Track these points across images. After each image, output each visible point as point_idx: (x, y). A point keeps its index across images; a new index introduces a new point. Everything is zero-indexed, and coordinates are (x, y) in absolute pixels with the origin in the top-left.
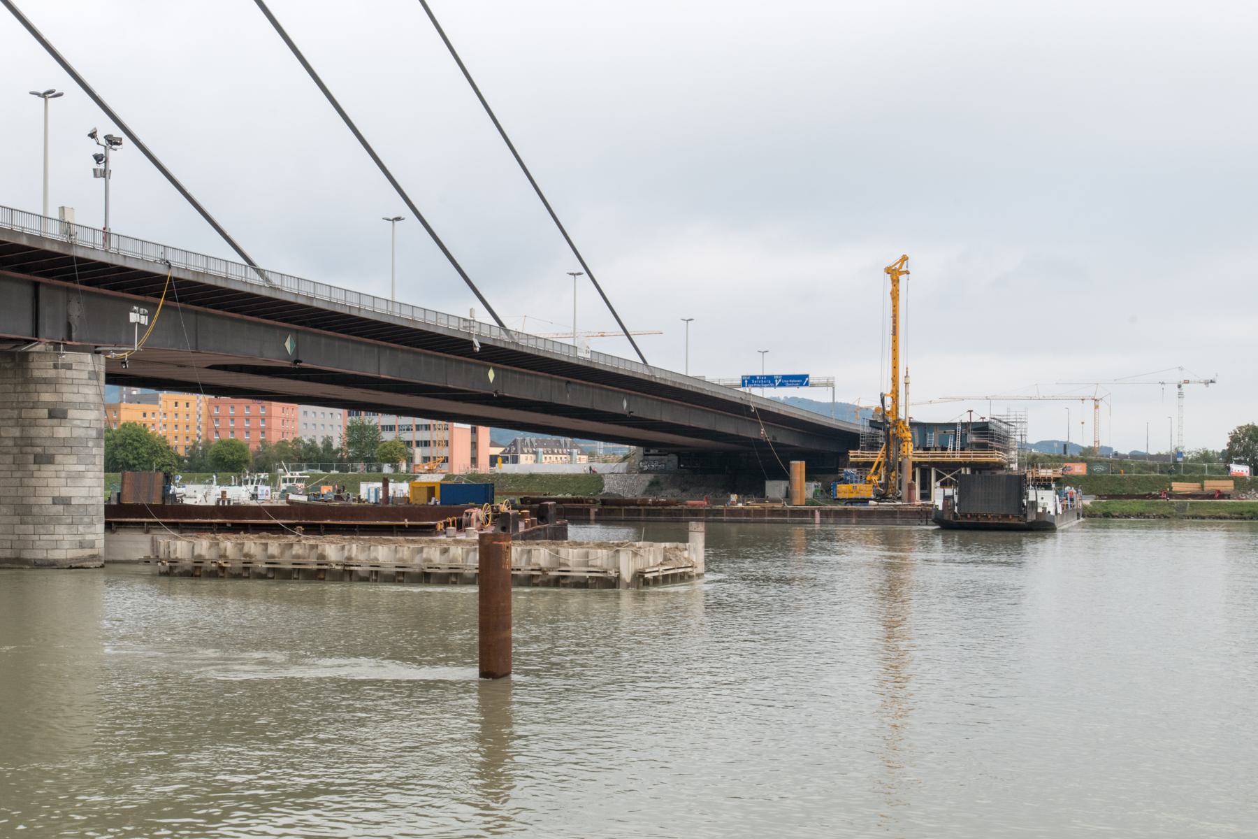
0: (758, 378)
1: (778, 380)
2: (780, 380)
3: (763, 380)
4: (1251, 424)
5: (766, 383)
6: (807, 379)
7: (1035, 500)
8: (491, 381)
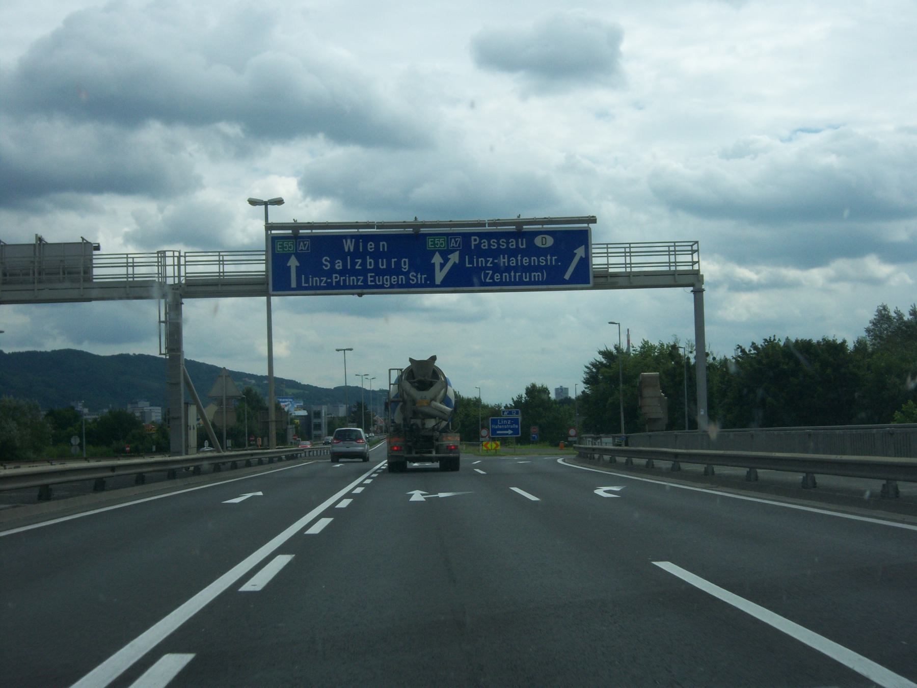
0: (349, 246)
1: (445, 254)
2: (454, 258)
3: (376, 255)
4: (831, 339)
5: (389, 272)
6: (580, 252)
7: (698, 269)
8: (331, 519)
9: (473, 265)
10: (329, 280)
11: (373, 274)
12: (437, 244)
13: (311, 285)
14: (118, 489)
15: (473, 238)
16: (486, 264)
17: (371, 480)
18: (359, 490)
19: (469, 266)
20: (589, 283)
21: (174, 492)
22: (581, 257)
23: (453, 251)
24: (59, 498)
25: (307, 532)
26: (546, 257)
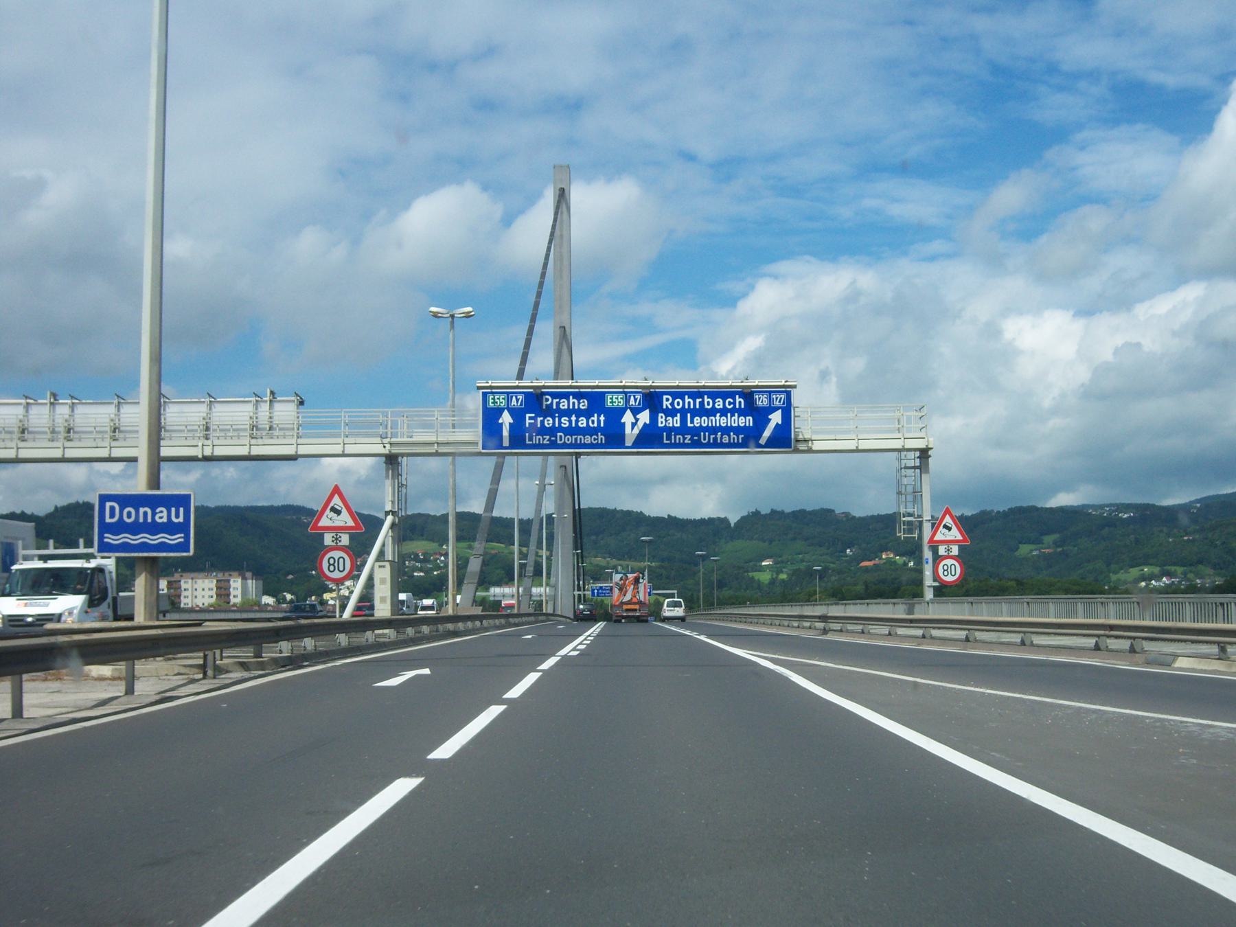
10: (553, 439)
11: (533, 415)
12: (615, 402)
15: (665, 397)
16: (684, 441)
20: (791, 448)
23: (776, 409)
24: (922, 513)
26: (570, 417)
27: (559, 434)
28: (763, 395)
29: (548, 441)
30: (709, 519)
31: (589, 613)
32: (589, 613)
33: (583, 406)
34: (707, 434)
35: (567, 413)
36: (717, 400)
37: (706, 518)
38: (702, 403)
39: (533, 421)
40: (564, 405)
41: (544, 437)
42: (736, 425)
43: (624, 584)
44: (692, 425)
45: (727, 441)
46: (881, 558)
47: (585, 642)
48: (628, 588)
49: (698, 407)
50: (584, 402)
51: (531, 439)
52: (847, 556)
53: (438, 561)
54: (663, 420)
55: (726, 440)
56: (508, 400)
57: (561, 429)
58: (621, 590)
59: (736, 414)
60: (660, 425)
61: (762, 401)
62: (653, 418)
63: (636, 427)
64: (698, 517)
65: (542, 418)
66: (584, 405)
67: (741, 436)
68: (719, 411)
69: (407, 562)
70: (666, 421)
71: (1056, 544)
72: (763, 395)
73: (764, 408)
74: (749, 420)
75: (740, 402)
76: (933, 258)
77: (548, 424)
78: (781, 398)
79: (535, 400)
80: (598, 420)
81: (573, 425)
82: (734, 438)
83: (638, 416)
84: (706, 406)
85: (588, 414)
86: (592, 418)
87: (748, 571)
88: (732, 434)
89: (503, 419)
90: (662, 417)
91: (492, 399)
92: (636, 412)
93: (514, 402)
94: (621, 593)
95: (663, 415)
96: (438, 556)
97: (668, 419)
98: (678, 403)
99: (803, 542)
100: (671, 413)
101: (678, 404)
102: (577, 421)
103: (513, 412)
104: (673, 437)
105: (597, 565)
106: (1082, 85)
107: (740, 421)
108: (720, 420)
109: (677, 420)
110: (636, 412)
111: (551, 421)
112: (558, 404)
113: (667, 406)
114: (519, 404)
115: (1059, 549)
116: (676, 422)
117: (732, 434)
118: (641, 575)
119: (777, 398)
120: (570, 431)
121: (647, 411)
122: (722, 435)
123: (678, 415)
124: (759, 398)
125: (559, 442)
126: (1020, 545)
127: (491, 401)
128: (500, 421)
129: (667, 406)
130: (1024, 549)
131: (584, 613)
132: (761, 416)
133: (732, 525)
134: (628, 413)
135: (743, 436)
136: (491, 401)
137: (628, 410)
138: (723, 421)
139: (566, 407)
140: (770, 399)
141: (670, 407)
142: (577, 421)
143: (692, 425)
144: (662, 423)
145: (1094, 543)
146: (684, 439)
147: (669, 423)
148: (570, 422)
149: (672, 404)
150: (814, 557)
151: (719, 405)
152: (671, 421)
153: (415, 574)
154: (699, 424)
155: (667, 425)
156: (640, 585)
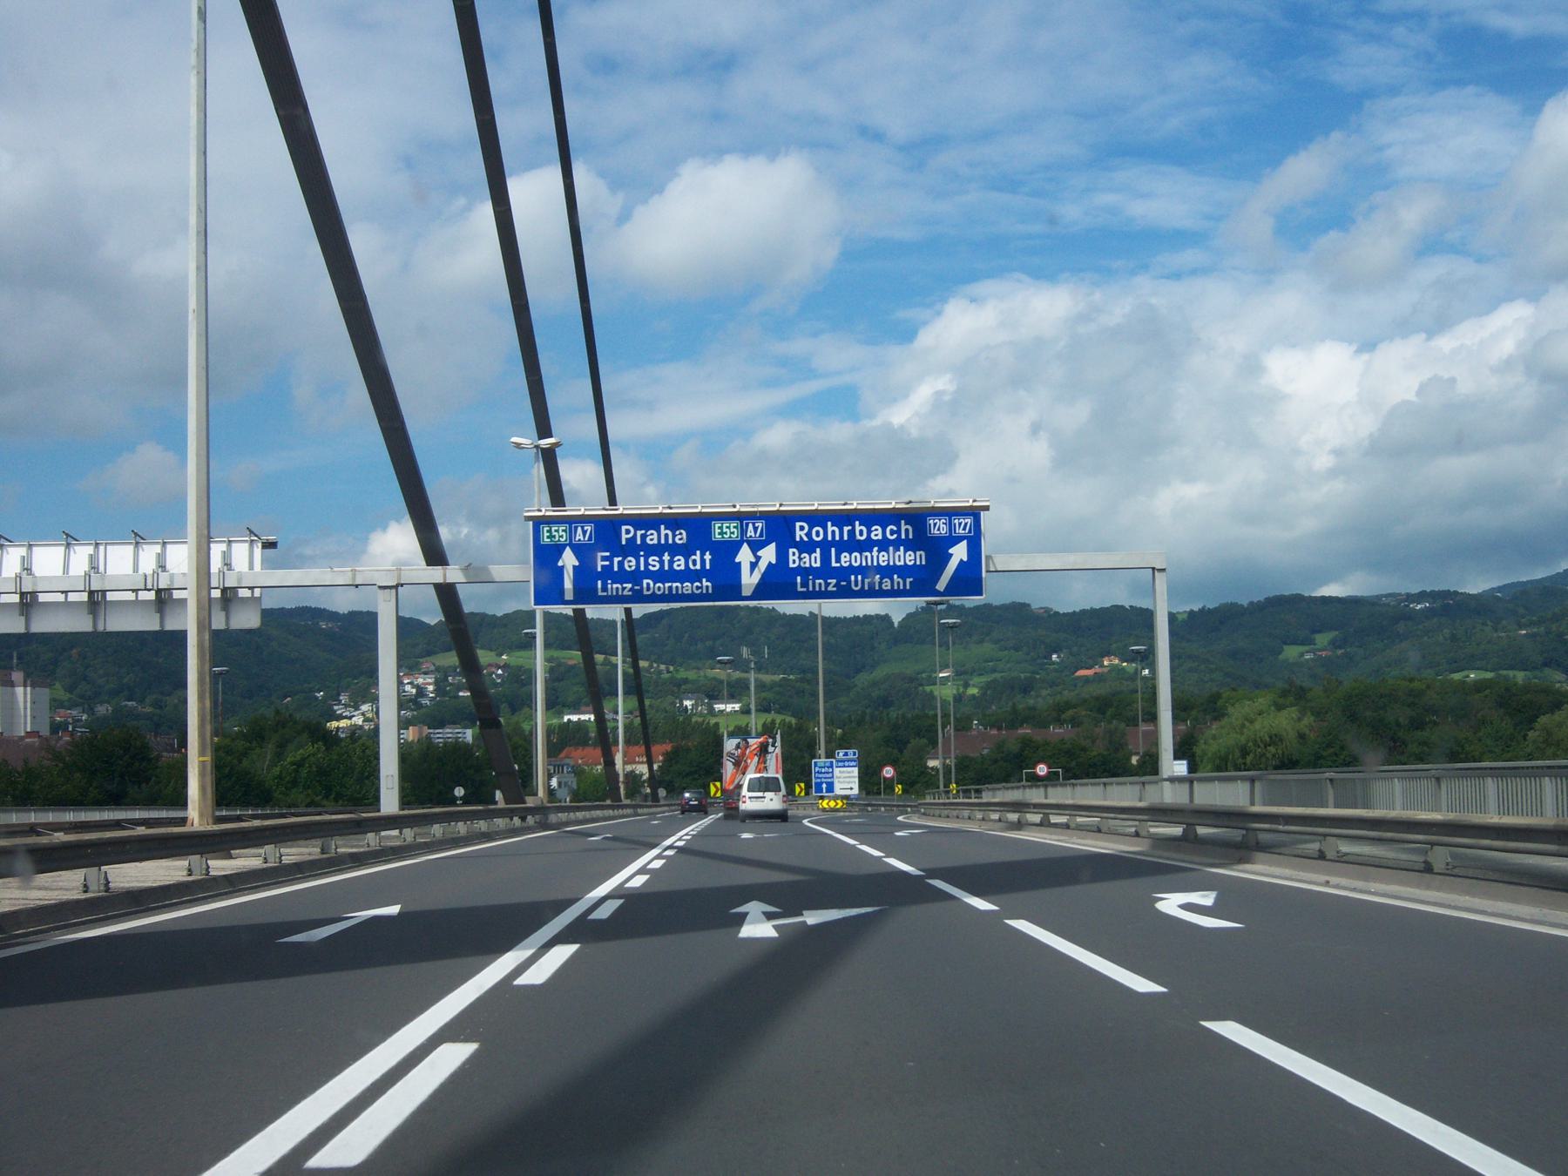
9: (808, 588)
11: (608, 554)
12: (726, 533)
13: (811, 589)
14: (1050, 552)
16: (826, 588)
17: (664, 861)
18: (658, 864)
19: (802, 590)
21: (483, 848)
22: (961, 560)
25: (591, 917)
26: (661, 556)
27: (645, 581)
28: (940, 520)
29: (629, 591)
30: (865, 616)
31: (696, 803)
32: (696, 803)
33: (680, 539)
34: (860, 577)
35: (658, 550)
36: (873, 528)
37: (861, 616)
38: (852, 533)
39: (607, 563)
40: (652, 538)
41: (625, 585)
42: (902, 563)
43: (743, 754)
44: (838, 565)
45: (889, 588)
46: (1102, 666)
47: (685, 838)
48: (749, 761)
49: (846, 538)
50: (681, 534)
51: (604, 589)
52: (1054, 663)
53: (494, 676)
54: (796, 558)
55: (887, 585)
56: (571, 533)
57: (648, 574)
58: (737, 764)
59: (902, 548)
60: (791, 565)
61: (939, 527)
62: (782, 555)
63: (757, 569)
64: (849, 615)
65: (620, 559)
66: (681, 537)
67: (908, 580)
68: (876, 543)
69: (450, 678)
70: (800, 559)
71: (1334, 644)
72: (940, 520)
73: (939, 539)
74: (921, 556)
75: (907, 530)
76: (1177, 276)
77: (630, 567)
78: (966, 524)
79: (607, 528)
80: (701, 560)
81: (666, 568)
82: (898, 583)
83: (759, 553)
84: (858, 537)
85: (686, 551)
86: (693, 557)
87: (922, 685)
88: (895, 576)
89: (563, 562)
90: (794, 554)
91: (548, 531)
92: (756, 546)
93: (579, 536)
94: (737, 770)
95: (795, 550)
96: (493, 669)
97: (802, 556)
98: (818, 534)
99: (993, 646)
100: (807, 547)
101: (818, 534)
102: (671, 562)
103: (578, 550)
104: (811, 582)
105: (714, 679)
106: (1399, 31)
107: (908, 558)
108: (878, 557)
109: (816, 558)
110: (756, 546)
111: (634, 563)
112: (644, 537)
113: (801, 537)
114: (586, 539)
115: (1340, 652)
116: (814, 560)
117: (895, 576)
118: (770, 740)
119: (960, 524)
120: (660, 576)
121: (773, 545)
122: (881, 579)
123: (818, 550)
124: (935, 524)
125: (645, 593)
126: (1285, 647)
127: (546, 534)
128: (560, 564)
129: (801, 537)
130: (1291, 652)
131: (691, 803)
132: (937, 551)
133: (896, 625)
134: (745, 549)
135: (911, 579)
136: (546, 534)
137: (745, 545)
138: (883, 559)
139: (655, 542)
140: (950, 526)
141: (806, 539)
142: (671, 562)
143: (838, 565)
144: (794, 562)
145: (1386, 641)
146: (827, 585)
147: (805, 563)
148: (661, 562)
149: (809, 534)
150: (1008, 665)
151: (876, 535)
152: (807, 560)
153: (461, 694)
154: (848, 563)
155: (802, 565)
156: (769, 756)
